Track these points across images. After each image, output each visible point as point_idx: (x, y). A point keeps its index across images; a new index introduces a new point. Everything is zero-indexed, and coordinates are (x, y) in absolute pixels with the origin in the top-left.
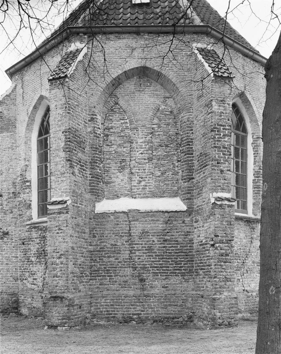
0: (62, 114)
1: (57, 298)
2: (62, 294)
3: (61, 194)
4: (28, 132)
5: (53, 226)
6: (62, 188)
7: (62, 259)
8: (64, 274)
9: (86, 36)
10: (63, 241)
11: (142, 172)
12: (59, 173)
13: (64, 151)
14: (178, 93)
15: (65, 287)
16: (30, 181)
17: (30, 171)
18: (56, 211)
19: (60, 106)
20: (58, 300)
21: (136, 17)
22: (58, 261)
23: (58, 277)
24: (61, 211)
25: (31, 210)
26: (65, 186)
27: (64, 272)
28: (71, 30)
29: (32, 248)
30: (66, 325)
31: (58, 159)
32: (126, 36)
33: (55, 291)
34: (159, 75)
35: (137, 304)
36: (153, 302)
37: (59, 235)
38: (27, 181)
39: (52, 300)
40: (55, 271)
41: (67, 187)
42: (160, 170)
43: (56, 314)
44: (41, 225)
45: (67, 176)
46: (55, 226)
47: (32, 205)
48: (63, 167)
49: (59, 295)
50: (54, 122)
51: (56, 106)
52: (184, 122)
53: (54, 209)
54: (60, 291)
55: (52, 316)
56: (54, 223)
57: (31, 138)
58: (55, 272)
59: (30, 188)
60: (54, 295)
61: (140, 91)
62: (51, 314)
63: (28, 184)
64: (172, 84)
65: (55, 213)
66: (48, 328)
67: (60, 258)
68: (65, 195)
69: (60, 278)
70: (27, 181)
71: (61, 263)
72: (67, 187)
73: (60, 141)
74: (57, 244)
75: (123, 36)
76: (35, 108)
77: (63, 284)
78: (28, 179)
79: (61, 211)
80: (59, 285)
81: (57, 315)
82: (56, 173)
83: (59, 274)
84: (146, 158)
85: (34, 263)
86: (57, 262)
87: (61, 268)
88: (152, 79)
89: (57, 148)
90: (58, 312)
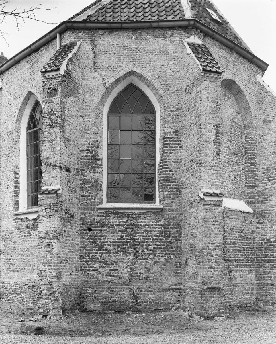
0: (213, 107)
1: (214, 289)
2: (217, 285)
3: (211, 186)
4: (101, 103)
5: (209, 217)
6: (212, 181)
7: (218, 250)
8: (219, 265)
9: (202, 34)
10: (219, 233)
11: (224, 174)
12: (209, 165)
13: (214, 144)
14: (248, 112)
15: (220, 278)
16: (101, 160)
17: (102, 149)
18: (212, 203)
19: (212, 99)
20: (215, 291)
21: (150, 15)
22: (213, 252)
23: (213, 268)
24: (217, 203)
25: (102, 192)
26: (215, 179)
27: (220, 263)
28: (196, 23)
29: (109, 235)
30: (223, 315)
31: (208, 151)
32: (225, 48)
33: (209, 282)
34: (240, 92)
35: (230, 293)
36: (238, 291)
37: (215, 227)
38: (99, 160)
39: (209, 292)
40: (210, 262)
41: (216, 180)
42: (233, 175)
43: (212, 305)
44: (127, 211)
45: (217, 169)
46: (211, 217)
47: (103, 186)
48: (213, 160)
49: (215, 286)
50: (205, 113)
51: (208, 97)
52: (251, 138)
53: (210, 201)
54: (215, 282)
55: (208, 307)
56: (211, 214)
57: (102, 111)
58: (210, 263)
59: (101, 168)
60: (210, 286)
61: (225, 100)
62: (208, 305)
63: (99, 162)
64: (246, 103)
65: (211, 204)
66: (205, 319)
67: (215, 249)
68: (214, 187)
69: (215, 269)
70: (99, 160)
71: (216, 255)
72: (216, 180)
73: (211, 134)
74: (212, 235)
75: (223, 47)
76: (118, 81)
77: (218, 275)
78: (100, 157)
79: (217, 203)
80: (214, 276)
81: (214, 305)
82: (206, 164)
83: (213, 266)
84: (227, 162)
85: (112, 252)
86: (212, 253)
87: (216, 259)
88: (232, 93)
89: (207, 140)
90: (215, 303)
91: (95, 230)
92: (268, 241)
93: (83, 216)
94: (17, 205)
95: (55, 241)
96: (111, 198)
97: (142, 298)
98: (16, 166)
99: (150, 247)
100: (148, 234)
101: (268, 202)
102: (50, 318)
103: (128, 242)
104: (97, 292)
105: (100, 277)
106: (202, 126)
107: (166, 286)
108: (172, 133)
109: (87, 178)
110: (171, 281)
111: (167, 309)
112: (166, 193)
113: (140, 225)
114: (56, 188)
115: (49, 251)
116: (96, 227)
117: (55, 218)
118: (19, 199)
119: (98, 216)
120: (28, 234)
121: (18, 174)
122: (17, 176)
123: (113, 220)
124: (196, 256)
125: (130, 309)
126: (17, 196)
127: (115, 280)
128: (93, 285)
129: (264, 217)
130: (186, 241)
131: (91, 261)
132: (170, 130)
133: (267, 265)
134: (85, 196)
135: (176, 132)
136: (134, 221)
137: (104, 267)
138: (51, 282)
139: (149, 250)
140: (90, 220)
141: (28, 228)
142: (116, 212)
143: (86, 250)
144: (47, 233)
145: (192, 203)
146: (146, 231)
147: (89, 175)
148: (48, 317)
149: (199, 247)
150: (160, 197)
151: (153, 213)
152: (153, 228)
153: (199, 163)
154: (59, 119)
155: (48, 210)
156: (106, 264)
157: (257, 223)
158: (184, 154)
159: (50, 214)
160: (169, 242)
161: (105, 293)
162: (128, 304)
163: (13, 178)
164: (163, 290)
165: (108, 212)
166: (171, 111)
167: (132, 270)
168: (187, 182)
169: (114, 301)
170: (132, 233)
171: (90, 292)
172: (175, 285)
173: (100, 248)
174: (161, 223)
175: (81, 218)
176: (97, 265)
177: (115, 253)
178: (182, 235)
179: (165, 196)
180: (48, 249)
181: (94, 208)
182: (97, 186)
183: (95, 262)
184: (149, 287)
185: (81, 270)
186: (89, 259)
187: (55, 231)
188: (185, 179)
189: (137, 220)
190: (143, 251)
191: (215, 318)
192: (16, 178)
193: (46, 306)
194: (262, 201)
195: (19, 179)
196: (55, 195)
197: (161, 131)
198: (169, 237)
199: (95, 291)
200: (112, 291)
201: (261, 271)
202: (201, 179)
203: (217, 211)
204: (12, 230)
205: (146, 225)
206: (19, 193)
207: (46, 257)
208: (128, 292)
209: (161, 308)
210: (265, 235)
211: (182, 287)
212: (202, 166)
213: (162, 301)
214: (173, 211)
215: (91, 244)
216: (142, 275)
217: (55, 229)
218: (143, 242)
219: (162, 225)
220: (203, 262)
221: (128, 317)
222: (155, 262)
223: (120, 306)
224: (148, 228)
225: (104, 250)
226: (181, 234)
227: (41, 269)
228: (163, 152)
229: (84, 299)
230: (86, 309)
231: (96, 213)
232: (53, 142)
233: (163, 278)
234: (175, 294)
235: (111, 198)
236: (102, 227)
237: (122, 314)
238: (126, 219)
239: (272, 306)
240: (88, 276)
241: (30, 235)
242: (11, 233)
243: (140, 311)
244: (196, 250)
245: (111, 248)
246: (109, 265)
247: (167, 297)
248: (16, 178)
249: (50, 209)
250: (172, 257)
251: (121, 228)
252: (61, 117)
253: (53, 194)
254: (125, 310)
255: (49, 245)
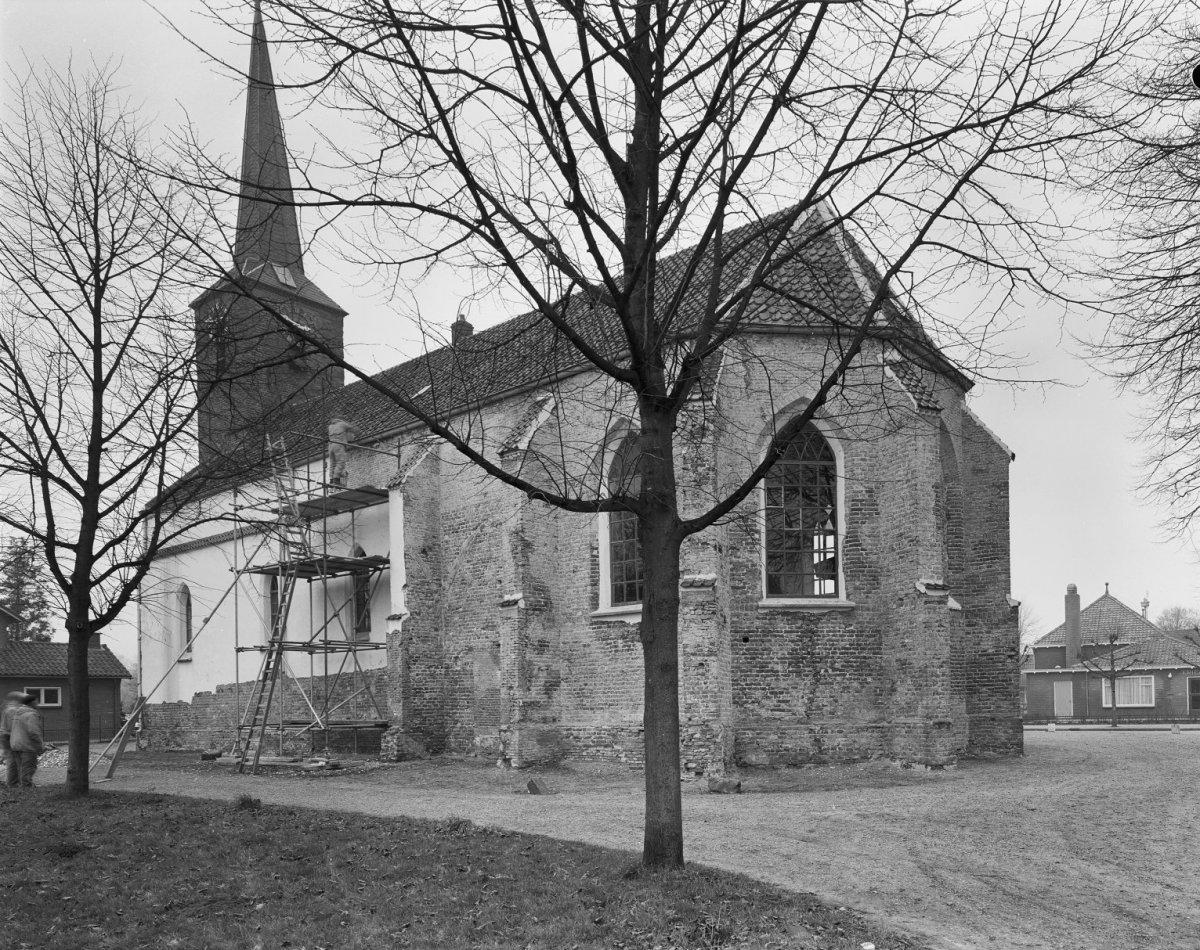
18: (936, 599)
49: (942, 720)
51: (924, 445)
56: (934, 616)
60: (936, 720)
74: (938, 646)
81: (943, 748)
83: (940, 690)
91: (755, 641)
92: (984, 653)
93: (735, 619)
94: (595, 601)
95: (713, 658)
96: (774, 589)
97: (827, 743)
98: (594, 535)
99: (837, 665)
100: (833, 645)
101: (981, 594)
102: (709, 775)
103: (805, 658)
104: (760, 736)
105: (764, 713)
106: (919, 487)
107: (862, 724)
108: (864, 492)
109: (740, 560)
110: (867, 716)
111: (865, 758)
112: (858, 583)
113: (821, 632)
114: (711, 576)
115: (703, 675)
116: (757, 636)
117: (712, 624)
118: (599, 589)
119: (758, 618)
120: (624, 646)
121: (597, 549)
122: (595, 552)
123: (782, 625)
124: (914, 676)
125: (810, 760)
126: (596, 585)
127: (786, 716)
128: (755, 725)
129: (976, 616)
130: (890, 657)
131: (749, 689)
132: (862, 488)
133: (984, 689)
134: (738, 588)
135: (870, 491)
136: (812, 626)
137: (768, 698)
138: (708, 721)
139: (834, 669)
140: (746, 625)
141: (623, 637)
142: (787, 613)
143: (741, 671)
144: (699, 646)
145: (901, 599)
146: (830, 640)
147: (744, 556)
148: (705, 774)
149: (918, 663)
150: (847, 589)
151: (841, 613)
152: (841, 636)
153: (915, 541)
154: (711, 473)
155: (700, 611)
156: (772, 693)
157: (967, 626)
158: (883, 525)
159: (703, 617)
160: (865, 657)
161: (773, 737)
162: (808, 753)
163: (588, 556)
164: (859, 730)
165: (773, 612)
166: (862, 460)
167: (811, 700)
168: (891, 568)
169: (786, 750)
170: (810, 644)
171: (751, 736)
172: (875, 722)
173: (763, 667)
174: (852, 628)
175: (733, 622)
176: (758, 694)
177: (785, 676)
178: (883, 646)
179: (856, 588)
180: (701, 671)
181: (751, 607)
182: (754, 572)
183: (755, 689)
184: (837, 726)
185: (734, 703)
186: (747, 685)
187: (712, 644)
188: (887, 562)
189: (816, 624)
190: (826, 671)
191: (945, 767)
192: (593, 556)
193: (700, 757)
194: (973, 591)
195: (598, 557)
196: (711, 589)
197: (847, 488)
198: (864, 649)
199: (758, 734)
200: (783, 734)
201: (975, 700)
202: (918, 563)
203: (942, 611)
204: (587, 641)
205: (830, 631)
206: (598, 580)
207: (697, 684)
208: (806, 734)
209: (856, 757)
210: (979, 644)
211: (885, 724)
212: (920, 545)
213: (857, 746)
214: (868, 610)
215: (748, 663)
216: (825, 708)
217: (711, 640)
218: (825, 657)
219: (853, 632)
220: (926, 685)
221: (812, 772)
222: (844, 688)
223: (796, 756)
224: (834, 636)
225: (768, 671)
226: (881, 644)
227: (689, 702)
228: (851, 521)
229: (742, 748)
230: (745, 763)
231: (754, 614)
232: (702, 506)
233: (857, 711)
234: (875, 735)
235: (774, 589)
236: (764, 636)
237: (800, 767)
238: (800, 623)
239: (994, 751)
240: (745, 712)
241: (628, 650)
242: (584, 646)
243: (825, 762)
244: (912, 668)
245: (779, 667)
246: (776, 693)
247: (864, 741)
248: (593, 556)
249: (703, 609)
250: (869, 679)
251: (794, 636)
252: (713, 470)
253: (707, 586)
254: (803, 762)
255: (702, 664)
